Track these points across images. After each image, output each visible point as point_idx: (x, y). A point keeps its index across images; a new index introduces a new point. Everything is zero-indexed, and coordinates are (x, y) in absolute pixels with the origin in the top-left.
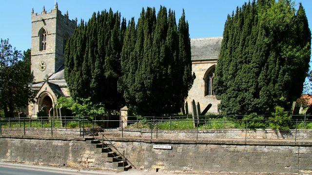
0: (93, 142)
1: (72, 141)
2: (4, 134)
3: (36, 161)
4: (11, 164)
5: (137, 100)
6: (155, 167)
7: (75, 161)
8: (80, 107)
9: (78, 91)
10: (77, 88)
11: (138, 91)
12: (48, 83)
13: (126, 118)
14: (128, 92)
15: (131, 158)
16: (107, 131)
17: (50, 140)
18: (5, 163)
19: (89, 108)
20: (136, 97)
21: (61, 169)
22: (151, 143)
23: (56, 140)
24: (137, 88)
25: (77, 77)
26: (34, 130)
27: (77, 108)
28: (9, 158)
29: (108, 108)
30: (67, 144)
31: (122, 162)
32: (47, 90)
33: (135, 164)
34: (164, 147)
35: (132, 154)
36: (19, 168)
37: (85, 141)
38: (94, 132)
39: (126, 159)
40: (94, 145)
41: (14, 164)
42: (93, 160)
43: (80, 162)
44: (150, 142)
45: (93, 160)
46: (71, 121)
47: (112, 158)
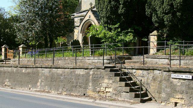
0: (111, 71)
1: (92, 70)
2: (37, 65)
3: (60, 90)
4: (39, 93)
5: (166, 23)
6: (173, 100)
7: (94, 91)
8: (110, 34)
9: (107, 18)
10: (106, 15)
11: (167, 14)
12: (92, 11)
13: (156, 44)
14: (157, 14)
15: (152, 89)
16: (135, 58)
17: (73, 69)
18: (35, 93)
19: (118, 34)
20: (165, 20)
21: (80, 99)
22: (169, 71)
23: (79, 69)
24: (166, 10)
25: (106, 4)
26: (65, 59)
27: (105, 36)
28: (39, 87)
29: (136, 34)
30: (88, 73)
31: (143, 96)
32: (91, 18)
33: (155, 95)
34: (184, 76)
35: (152, 84)
36: (44, 97)
37: (104, 69)
38: (121, 60)
39: (146, 90)
40: (112, 74)
41: (42, 94)
42: (110, 90)
43: (99, 92)
44: (168, 70)
45: (110, 90)
46: (100, 49)
47: (128, 88)
